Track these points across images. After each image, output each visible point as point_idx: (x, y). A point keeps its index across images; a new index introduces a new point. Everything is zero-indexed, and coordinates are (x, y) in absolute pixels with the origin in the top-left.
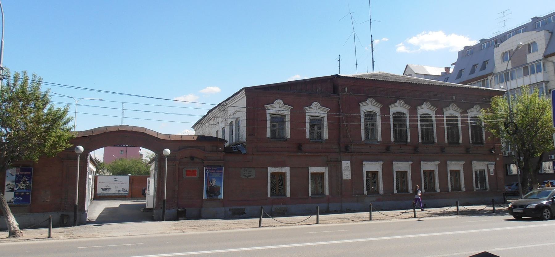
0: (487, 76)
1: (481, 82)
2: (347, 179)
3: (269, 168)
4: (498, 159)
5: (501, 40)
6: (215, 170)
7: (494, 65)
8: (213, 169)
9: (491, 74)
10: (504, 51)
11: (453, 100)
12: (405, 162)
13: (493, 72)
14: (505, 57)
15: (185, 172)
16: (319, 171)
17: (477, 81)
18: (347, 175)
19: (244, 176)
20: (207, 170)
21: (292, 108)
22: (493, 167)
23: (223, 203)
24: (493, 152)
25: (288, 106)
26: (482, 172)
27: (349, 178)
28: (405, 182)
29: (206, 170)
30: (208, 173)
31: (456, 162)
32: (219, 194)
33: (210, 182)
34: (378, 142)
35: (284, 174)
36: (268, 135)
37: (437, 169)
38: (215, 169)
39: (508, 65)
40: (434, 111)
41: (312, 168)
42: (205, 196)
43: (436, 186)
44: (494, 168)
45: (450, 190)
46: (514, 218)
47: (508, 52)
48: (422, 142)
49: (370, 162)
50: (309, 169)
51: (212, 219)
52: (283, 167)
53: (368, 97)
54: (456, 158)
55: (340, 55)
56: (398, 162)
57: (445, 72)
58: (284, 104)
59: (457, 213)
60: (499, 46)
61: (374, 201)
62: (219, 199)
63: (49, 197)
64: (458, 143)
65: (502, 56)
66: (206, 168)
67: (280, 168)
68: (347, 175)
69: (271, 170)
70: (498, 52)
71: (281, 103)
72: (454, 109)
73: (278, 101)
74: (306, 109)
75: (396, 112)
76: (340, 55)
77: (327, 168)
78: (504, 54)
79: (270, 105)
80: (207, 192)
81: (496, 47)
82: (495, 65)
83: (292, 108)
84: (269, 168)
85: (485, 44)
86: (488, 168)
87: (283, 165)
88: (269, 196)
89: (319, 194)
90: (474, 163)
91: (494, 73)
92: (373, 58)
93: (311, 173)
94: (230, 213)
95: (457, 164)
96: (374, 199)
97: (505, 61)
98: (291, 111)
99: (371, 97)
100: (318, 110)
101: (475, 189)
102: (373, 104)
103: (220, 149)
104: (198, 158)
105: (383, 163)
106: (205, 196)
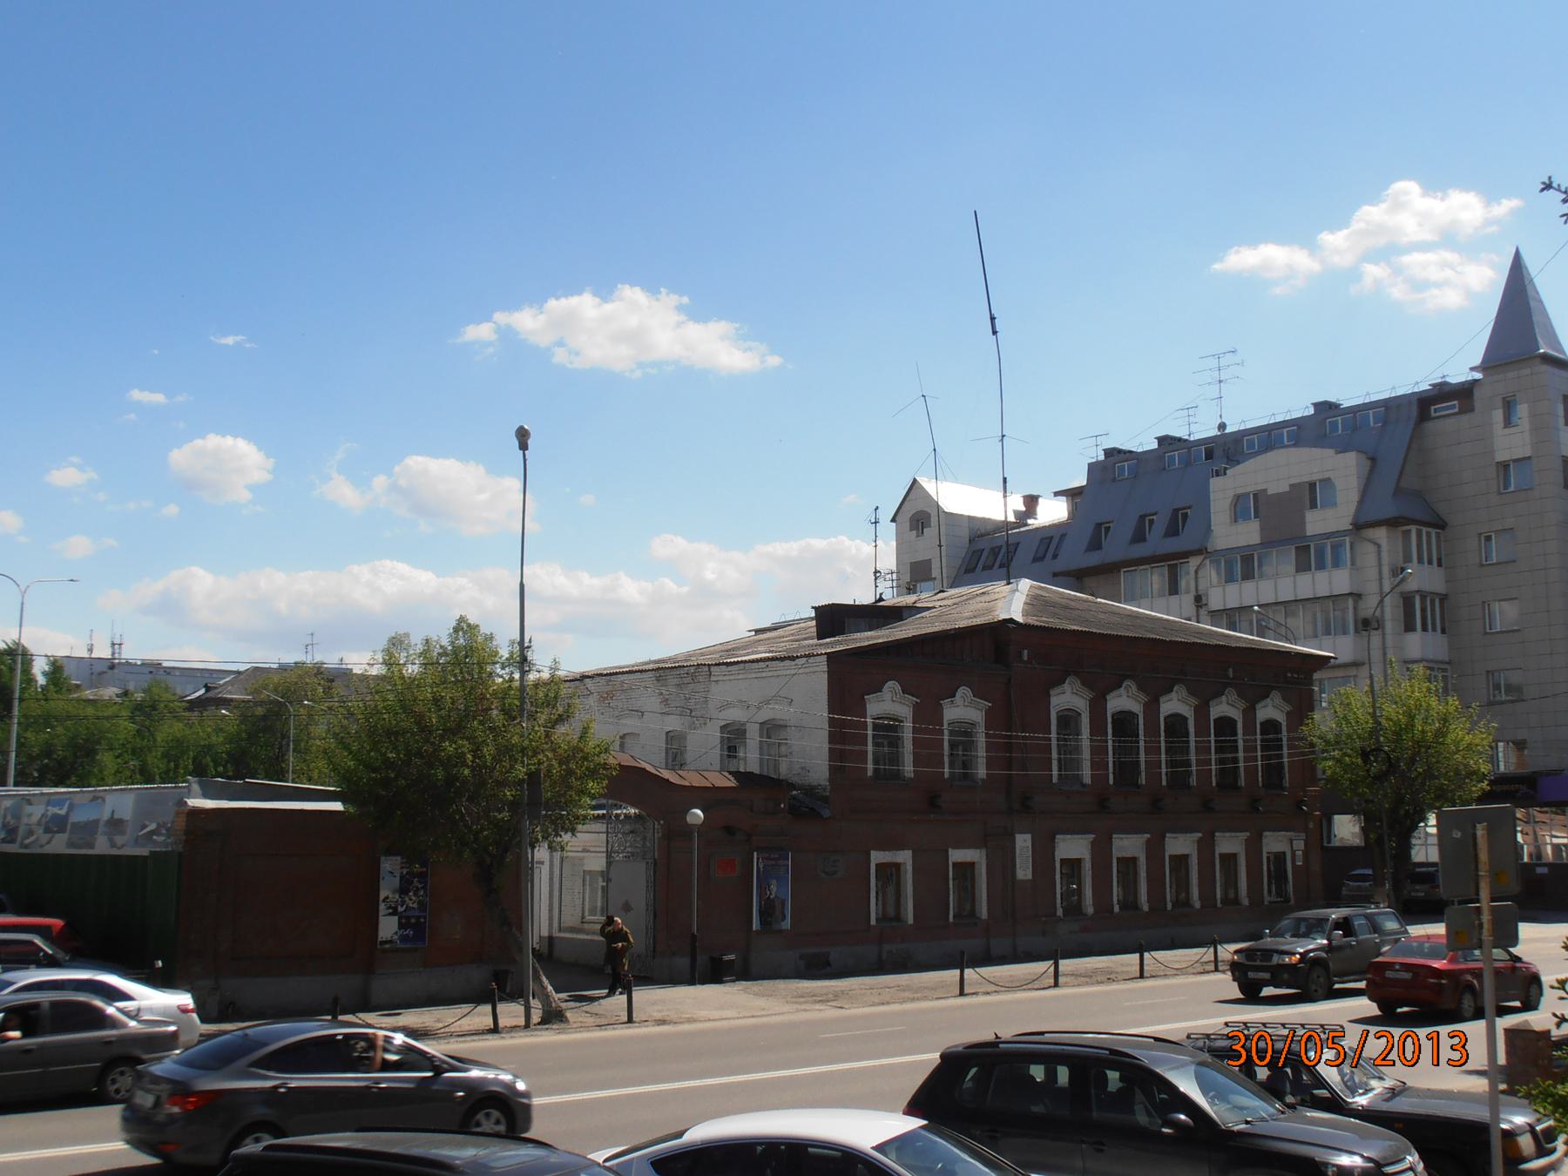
0: (1186, 555)
1: (1166, 568)
2: (1025, 878)
3: (873, 854)
4: (1311, 825)
5: (1224, 450)
7: (1210, 526)
8: (772, 856)
9: (1201, 551)
10: (1240, 491)
12: (1135, 836)
13: (1206, 549)
14: (1242, 507)
16: (969, 859)
17: (1152, 565)
18: (1024, 872)
20: (760, 860)
21: (918, 701)
24: (1304, 808)
25: (910, 697)
26: (1279, 858)
28: (1182, 883)
29: (758, 859)
30: (761, 866)
34: (1084, 786)
35: (897, 866)
37: (1196, 852)
39: (1248, 533)
40: (1191, 706)
41: (956, 851)
42: (756, 925)
43: (1085, 895)
45: (1219, 905)
46: (1242, 996)
47: (1252, 496)
50: (950, 853)
51: (776, 979)
52: (900, 850)
56: (1121, 836)
57: (1023, 509)
58: (903, 693)
60: (1225, 474)
62: (781, 931)
65: (1232, 501)
66: (758, 854)
67: (894, 852)
68: (1024, 872)
69: (877, 857)
70: (1223, 490)
71: (896, 688)
72: (1230, 702)
73: (890, 683)
75: (1118, 709)
77: (984, 852)
78: (1239, 499)
79: (874, 695)
80: (762, 913)
81: (1217, 475)
82: (1212, 528)
83: (918, 701)
84: (873, 854)
85: (1176, 453)
86: (1292, 847)
90: (1266, 836)
91: (1209, 550)
93: (953, 864)
97: (1240, 521)
98: (916, 707)
100: (967, 706)
101: (1267, 899)
102: (1075, 691)
105: (1095, 839)
106: (756, 925)
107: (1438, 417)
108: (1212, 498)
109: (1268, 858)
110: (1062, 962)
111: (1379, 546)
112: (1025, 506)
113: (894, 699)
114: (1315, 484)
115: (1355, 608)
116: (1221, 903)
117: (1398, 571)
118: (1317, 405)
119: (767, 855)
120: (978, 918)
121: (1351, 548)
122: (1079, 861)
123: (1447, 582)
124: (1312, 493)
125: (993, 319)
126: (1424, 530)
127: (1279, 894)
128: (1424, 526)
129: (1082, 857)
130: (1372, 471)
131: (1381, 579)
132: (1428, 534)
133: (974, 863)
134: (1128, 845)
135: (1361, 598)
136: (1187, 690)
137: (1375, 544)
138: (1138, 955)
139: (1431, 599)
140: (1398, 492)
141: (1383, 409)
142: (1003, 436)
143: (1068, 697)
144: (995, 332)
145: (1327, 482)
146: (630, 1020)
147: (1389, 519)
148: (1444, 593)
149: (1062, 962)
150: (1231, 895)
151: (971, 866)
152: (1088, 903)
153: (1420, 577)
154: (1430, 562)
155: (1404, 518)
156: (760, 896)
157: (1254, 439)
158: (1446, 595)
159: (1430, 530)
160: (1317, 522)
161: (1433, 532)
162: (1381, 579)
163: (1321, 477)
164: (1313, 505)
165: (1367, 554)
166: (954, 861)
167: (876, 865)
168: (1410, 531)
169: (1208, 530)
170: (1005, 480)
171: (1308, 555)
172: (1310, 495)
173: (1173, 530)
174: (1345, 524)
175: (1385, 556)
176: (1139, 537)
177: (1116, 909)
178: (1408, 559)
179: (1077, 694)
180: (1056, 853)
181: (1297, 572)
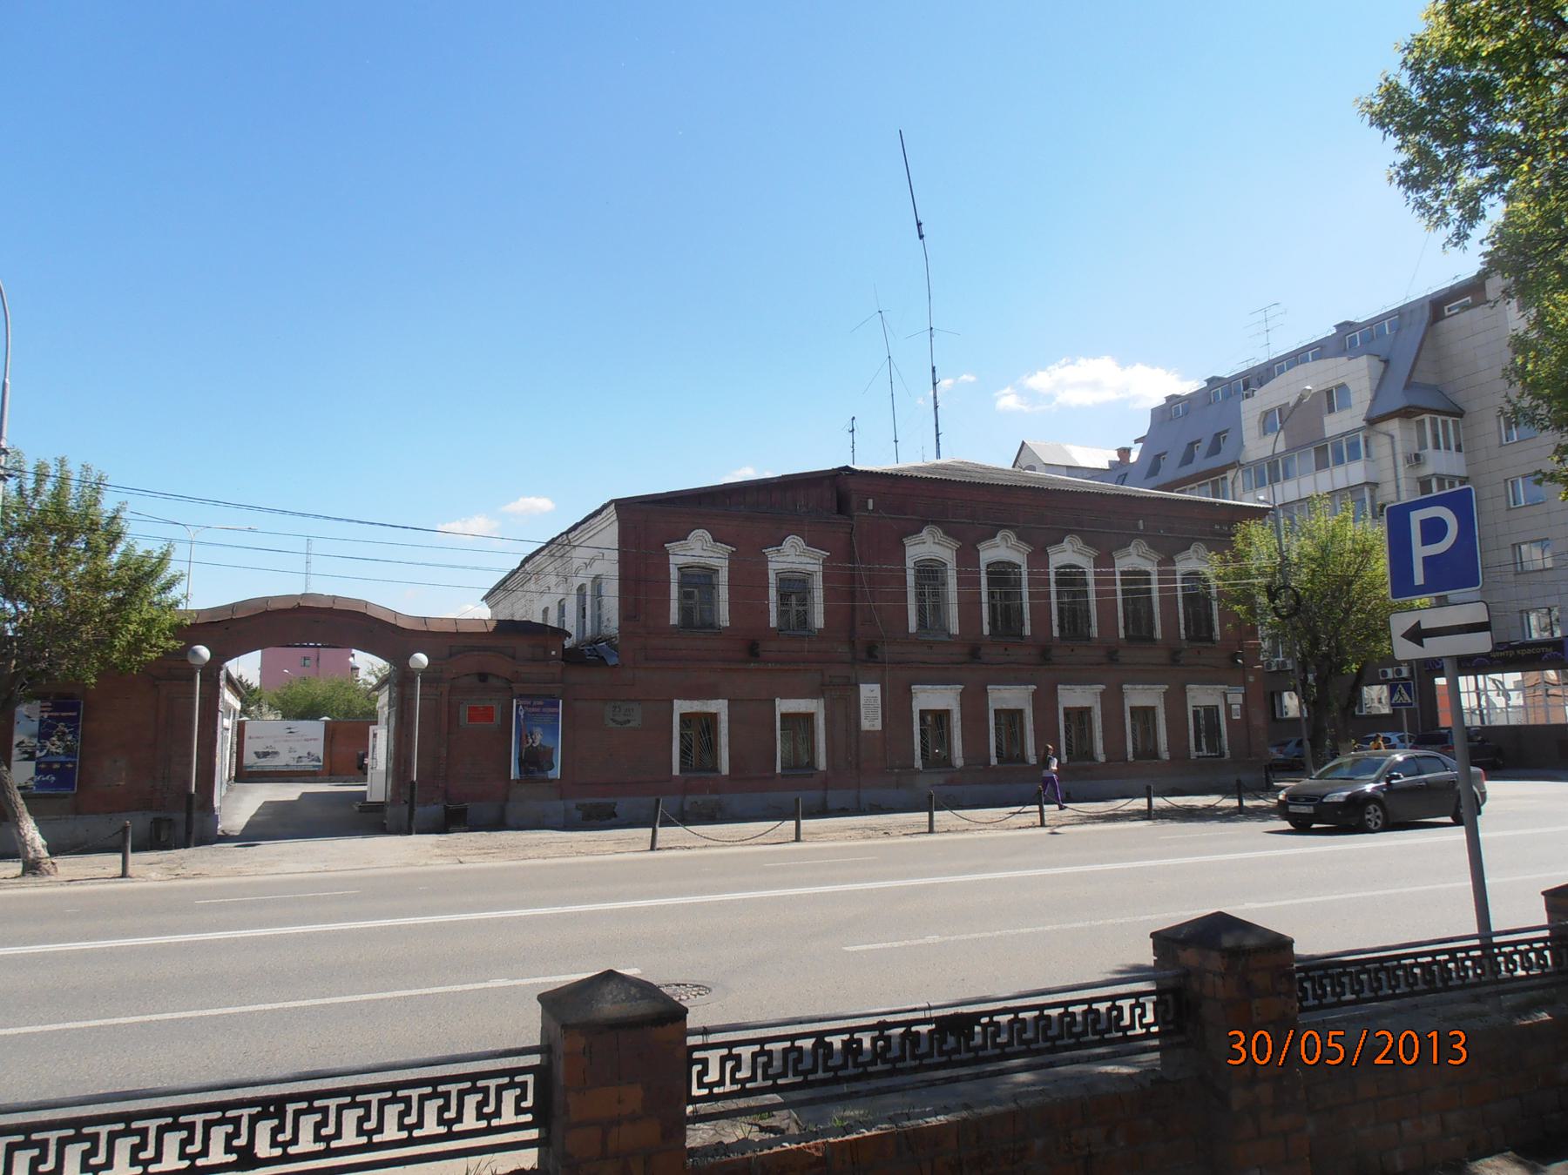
0: (1224, 469)
2: (872, 729)
3: (677, 703)
4: (1251, 679)
6: (541, 707)
8: (535, 703)
9: (1232, 466)
11: (1138, 530)
13: (1239, 461)
14: (1268, 422)
15: (464, 713)
18: (871, 720)
19: (614, 721)
20: (521, 707)
22: (1240, 699)
23: (560, 789)
24: (1239, 661)
25: (723, 545)
27: (878, 726)
29: (518, 707)
30: (522, 714)
31: (1146, 687)
32: (552, 767)
33: (527, 736)
34: (950, 636)
36: (674, 618)
38: (541, 703)
40: (1090, 557)
42: (514, 773)
44: (1241, 702)
46: (1292, 828)
47: (1277, 411)
48: (1061, 637)
49: (929, 687)
52: (712, 699)
53: (926, 523)
54: (1145, 676)
55: (853, 418)
59: (1148, 815)
60: (1253, 395)
61: (939, 785)
63: (124, 774)
64: (1152, 639)
65: (1260, 419)
66: (517, 702)
68: (871, 720)
69: (681, 706)
70: (1251, 409)
71: (706, 537)
74: (770, 552)
75: (995, 559)
76: (853, 418)
78: (1267, 415)
79: (678, 543)
83: (734, 549)
84: (677, 703)
86: (1226, 700)
87: (713, 695)
88: (676, 771)
89: (801, 767)
91: (1241, 462)
92: (937, 425)
93: (782, 715)
94: (579, 814)
95: (1148, 691)
96: (940, 779)
98: (732, 558)
99: (933, 522)
101: (1194, 754)
102: (936, 541)
103: (553, 653)
104: (498, 677)
105: (963, 690)
106: (514, 773)
107: (1449, 316)
108: (1243, 418)
109: (1196, 713)
110: (803, 822)
111: (1392, 437)
112: (1119, 456)
113: (705, 548)
114: (1332, 391)
115: (1372, 497)
116: (1134, 756)
117: (1416, 459)
118: (1337, 326)
119: (529, 703)
120: (816, 770)
121: (1367, 446)
122: (947, 712)
123: (1467, 465)
124: (1332, 398)
125: (919, 224)
126: (1440, 419)
127: (1211, 747)
128: (1440, 415)
129: (949, 708)
130: (1385, 371)
131: (1395, 466)
132: (1445, 423)
133: (813, 714)
134: (1009, 696)
135: (1378, 487)
136: (1083, 541)
137: (1389, 435)
138: (794, 822)
139: (1449, 482)
140: (1409, 385)
141: (1397, 317)
142: (931, 329)
143: (927, 546)
144: (921, 237)
145: (1342, 387)
146: (652, 849)
147: (1400, 410)
148: (1466, 475)
149: (803, 822)
150: (1017, 751)
151: (809, 718)
152: (956, 756)
153: (1442, 462)
154: (1448, 448)
155: (1415, 407)
156: (520, 742)
157: (1283, 365)
158: (1467, 478)
159: (1444, 418)
160: (1335, 424)
161: (1450, 420)
162: (1395, 466)
163: (1335, 383)
164: (1331, 410)
165: (1381, 447)
166: (784, 711)
167: (681, 715)
168: (1423, 420)
169: (1242, 445)
170: (934, 369)
171: (1326, 453)
172: (1328, 401)
173: (1215, 449)
174: (1361, 423)
175: (1399, 449)
176: (1188, 458)
177: (994, 761)
178: (1423, 446)
179: (939, 544)
180: (914, 703)
181: (1317, 470)
